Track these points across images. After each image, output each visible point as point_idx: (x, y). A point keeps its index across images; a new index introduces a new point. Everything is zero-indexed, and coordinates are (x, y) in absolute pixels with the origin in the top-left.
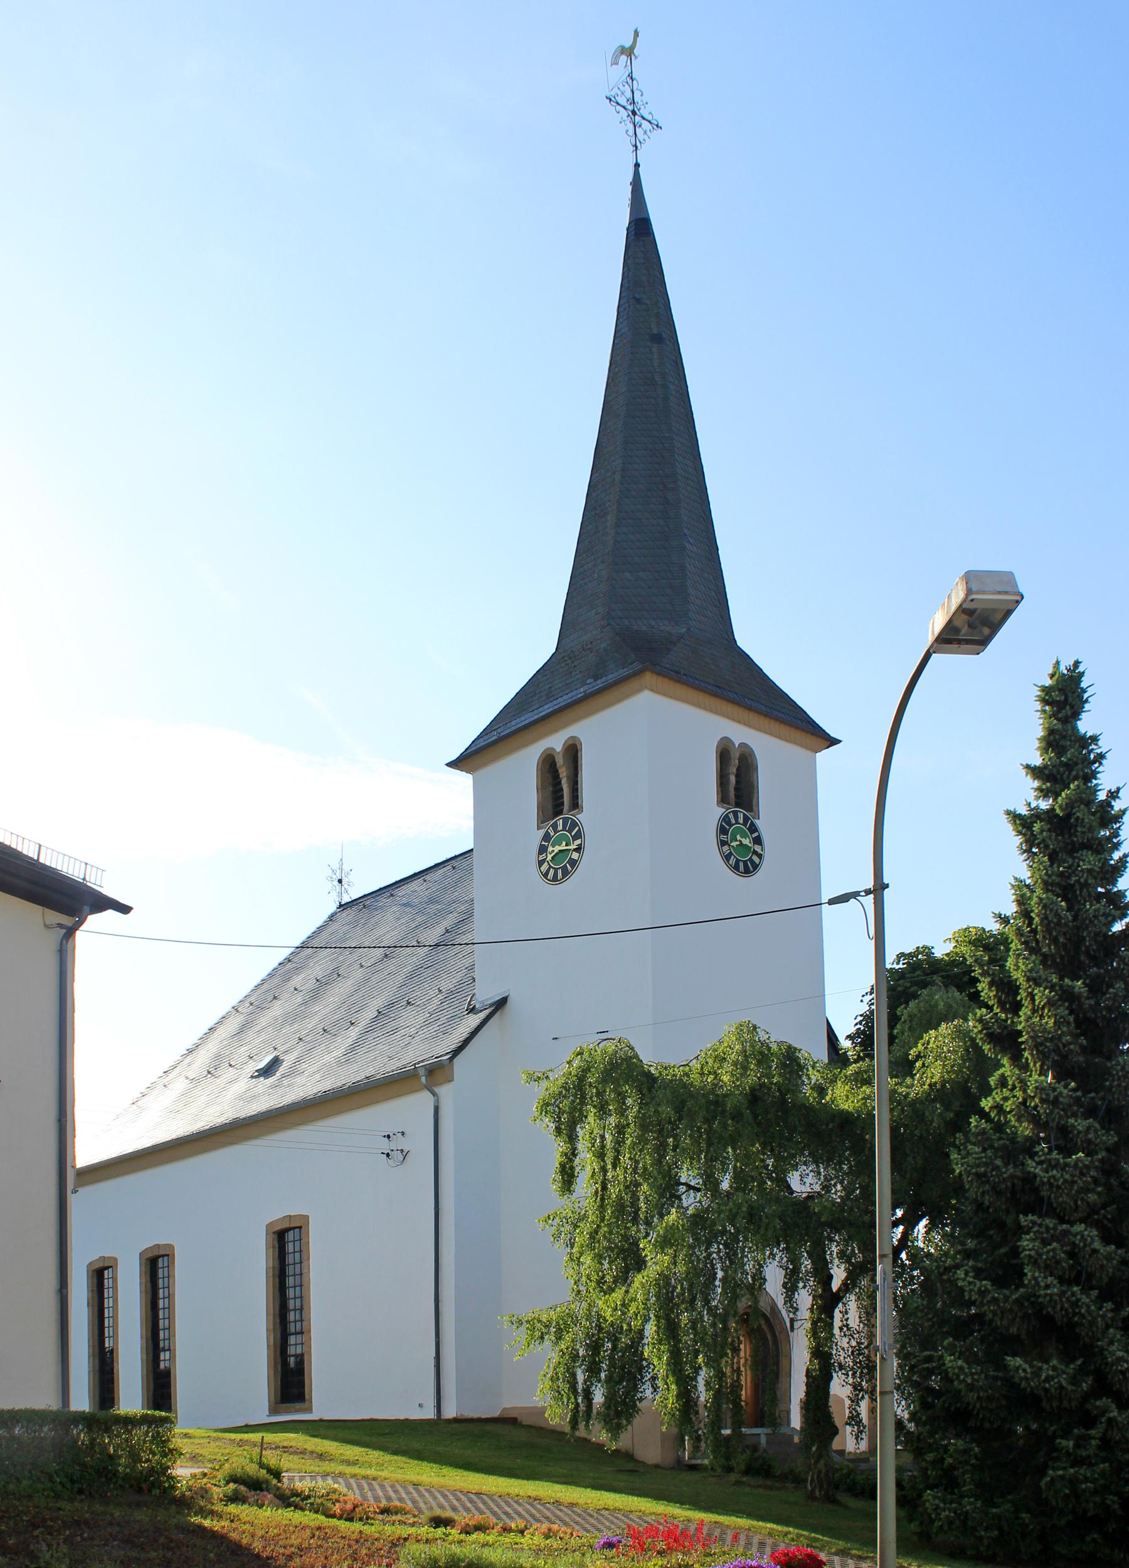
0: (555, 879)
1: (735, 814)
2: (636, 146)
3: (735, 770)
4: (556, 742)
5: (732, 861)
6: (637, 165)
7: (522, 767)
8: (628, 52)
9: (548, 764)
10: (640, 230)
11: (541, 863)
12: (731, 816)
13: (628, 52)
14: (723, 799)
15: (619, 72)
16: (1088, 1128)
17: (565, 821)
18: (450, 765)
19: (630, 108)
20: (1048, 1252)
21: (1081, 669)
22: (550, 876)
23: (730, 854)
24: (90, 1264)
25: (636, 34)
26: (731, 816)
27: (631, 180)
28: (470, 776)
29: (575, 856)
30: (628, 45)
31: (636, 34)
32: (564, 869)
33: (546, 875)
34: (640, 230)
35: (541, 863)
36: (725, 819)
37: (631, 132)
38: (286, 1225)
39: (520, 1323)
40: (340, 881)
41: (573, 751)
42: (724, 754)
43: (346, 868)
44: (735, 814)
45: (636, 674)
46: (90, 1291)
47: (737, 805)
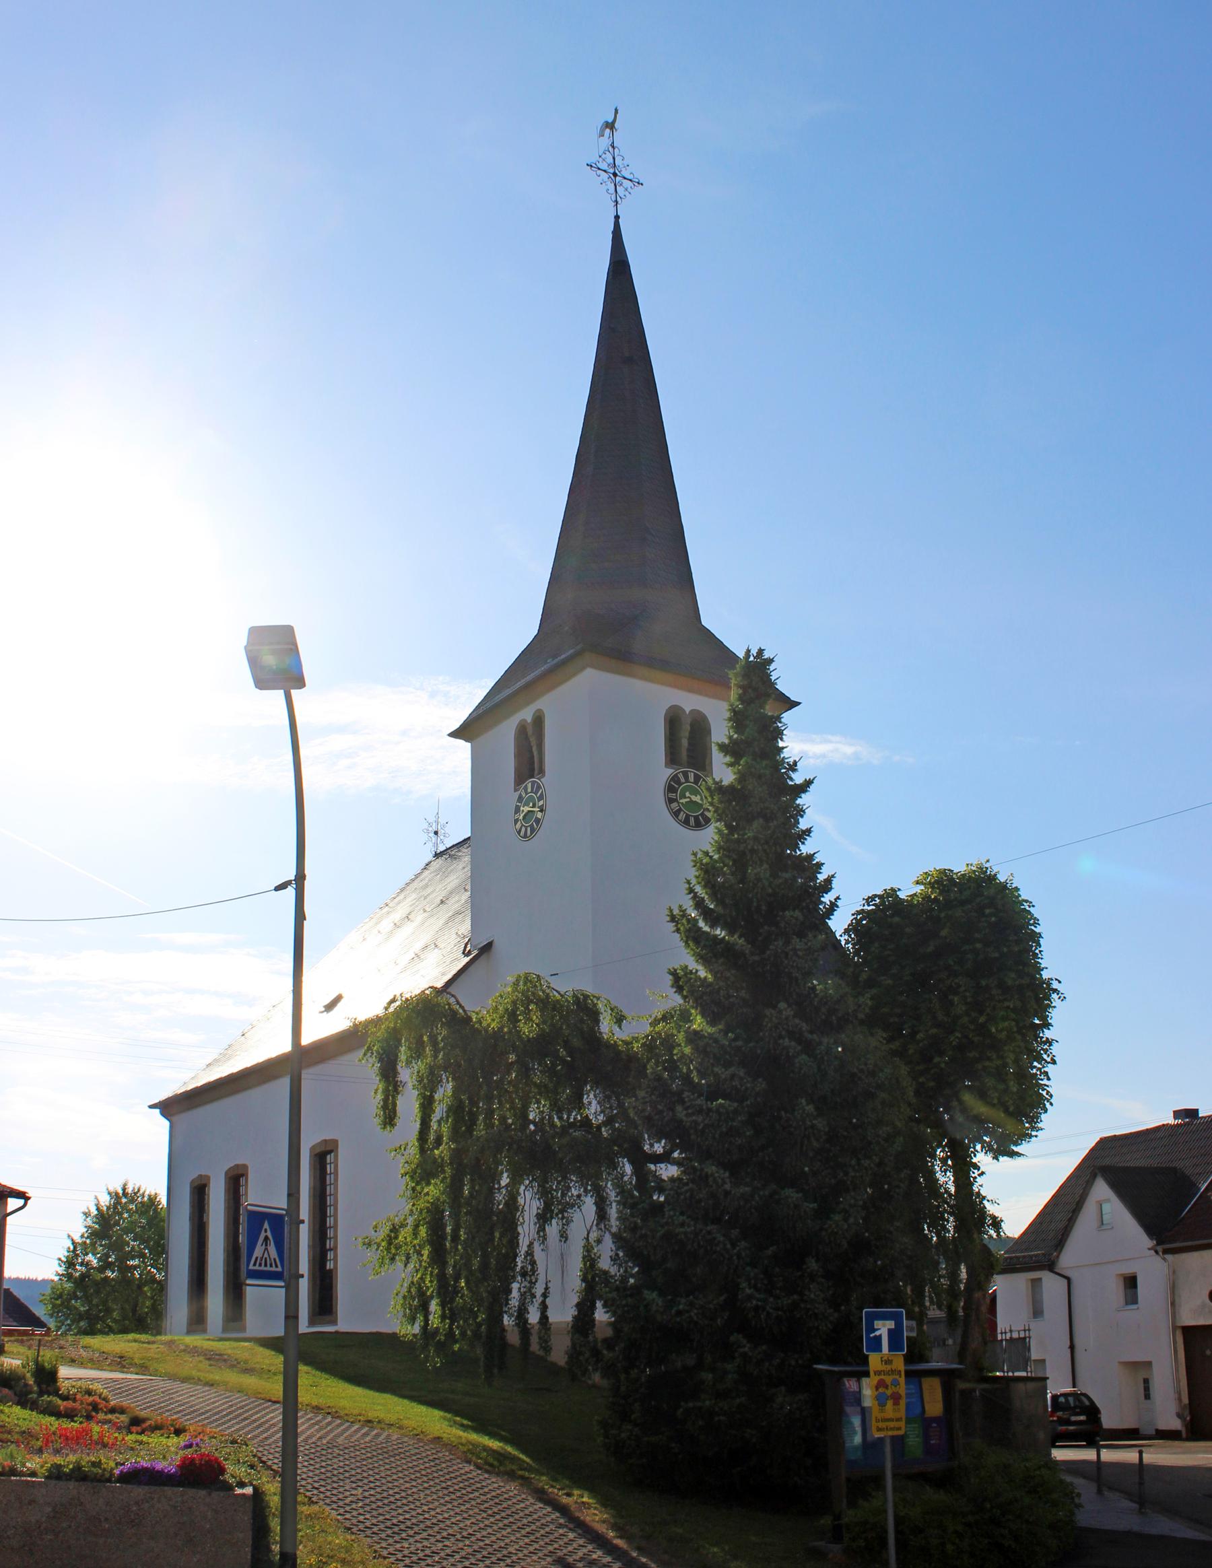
0: (525, 836)
1: (685, 774)
2: (616, 202)
3: (687, 734)
4: (527, 714)
5: (682, 816)
6: (617, 217)
7: (505, 734)
8: (611, 126)
9: (522, 730)
10: (619, 269)
11: (516, 821)
12: (680, 776)
13: (611, 126)
14: (672, 758)
15: (605, 142)
16: (733, 1076)
17: (533, 783)
18: (455, 734)
19: (612, 171)
20: (687, 1191)
21: (766, 655)
22: (522, 833)
23: (680, 810)
24: (192, 1182)
25: (616, 111)
26: (680, 776)
27: (612, 229)
28: (469, 745)
29: (539, 815)
30: (610, 120)
31: (616, 111)
32: (532, 826)
33: (519, 832)
34: (619, 269)
35: (516, 821)
36: (675, 778)
37: (612, 190)
38: (323, 1149)
39: (369, 1244)
40: (436, 833)
41: (539, 720)
42: (673, 720)
43: (442, 821)
44: (685, 774)
45: (578, 654)
46: (192, 1206)
47: (690, 765)
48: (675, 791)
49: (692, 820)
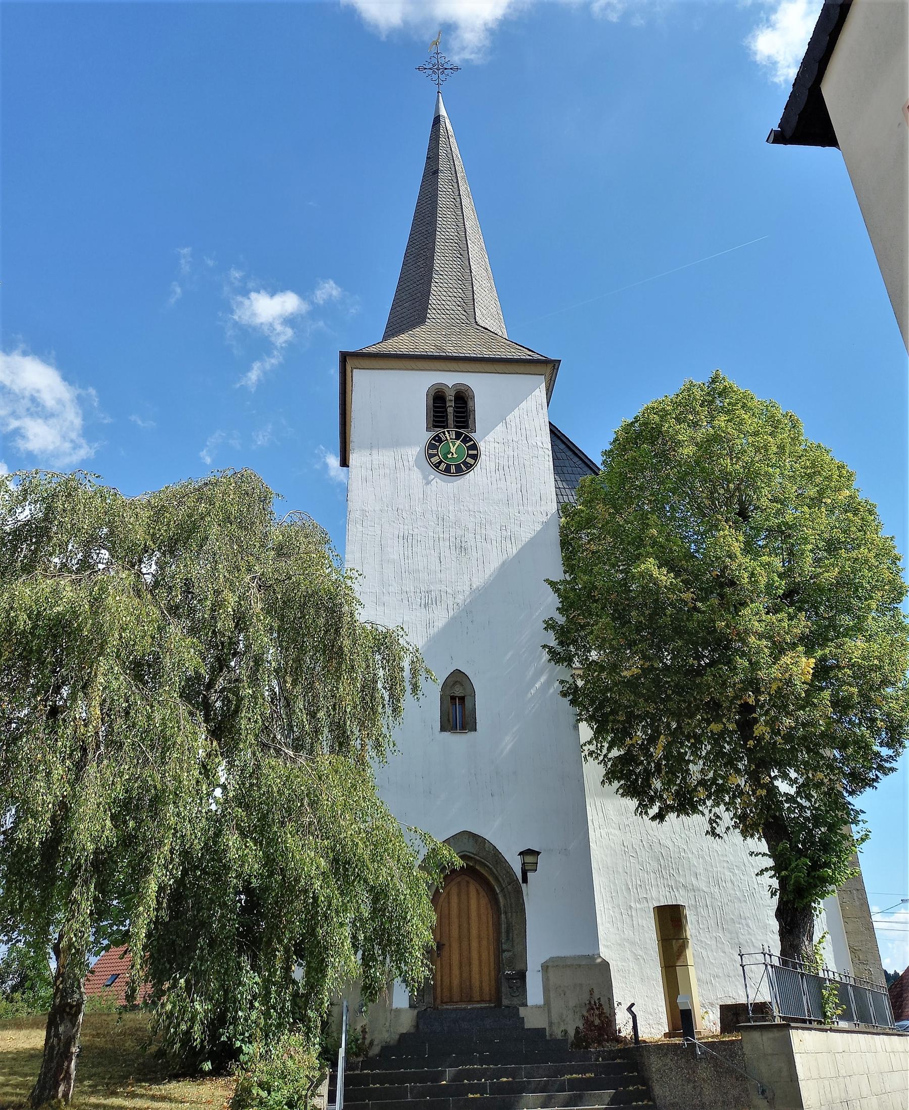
48: (436, 448)
49: (453, 469)
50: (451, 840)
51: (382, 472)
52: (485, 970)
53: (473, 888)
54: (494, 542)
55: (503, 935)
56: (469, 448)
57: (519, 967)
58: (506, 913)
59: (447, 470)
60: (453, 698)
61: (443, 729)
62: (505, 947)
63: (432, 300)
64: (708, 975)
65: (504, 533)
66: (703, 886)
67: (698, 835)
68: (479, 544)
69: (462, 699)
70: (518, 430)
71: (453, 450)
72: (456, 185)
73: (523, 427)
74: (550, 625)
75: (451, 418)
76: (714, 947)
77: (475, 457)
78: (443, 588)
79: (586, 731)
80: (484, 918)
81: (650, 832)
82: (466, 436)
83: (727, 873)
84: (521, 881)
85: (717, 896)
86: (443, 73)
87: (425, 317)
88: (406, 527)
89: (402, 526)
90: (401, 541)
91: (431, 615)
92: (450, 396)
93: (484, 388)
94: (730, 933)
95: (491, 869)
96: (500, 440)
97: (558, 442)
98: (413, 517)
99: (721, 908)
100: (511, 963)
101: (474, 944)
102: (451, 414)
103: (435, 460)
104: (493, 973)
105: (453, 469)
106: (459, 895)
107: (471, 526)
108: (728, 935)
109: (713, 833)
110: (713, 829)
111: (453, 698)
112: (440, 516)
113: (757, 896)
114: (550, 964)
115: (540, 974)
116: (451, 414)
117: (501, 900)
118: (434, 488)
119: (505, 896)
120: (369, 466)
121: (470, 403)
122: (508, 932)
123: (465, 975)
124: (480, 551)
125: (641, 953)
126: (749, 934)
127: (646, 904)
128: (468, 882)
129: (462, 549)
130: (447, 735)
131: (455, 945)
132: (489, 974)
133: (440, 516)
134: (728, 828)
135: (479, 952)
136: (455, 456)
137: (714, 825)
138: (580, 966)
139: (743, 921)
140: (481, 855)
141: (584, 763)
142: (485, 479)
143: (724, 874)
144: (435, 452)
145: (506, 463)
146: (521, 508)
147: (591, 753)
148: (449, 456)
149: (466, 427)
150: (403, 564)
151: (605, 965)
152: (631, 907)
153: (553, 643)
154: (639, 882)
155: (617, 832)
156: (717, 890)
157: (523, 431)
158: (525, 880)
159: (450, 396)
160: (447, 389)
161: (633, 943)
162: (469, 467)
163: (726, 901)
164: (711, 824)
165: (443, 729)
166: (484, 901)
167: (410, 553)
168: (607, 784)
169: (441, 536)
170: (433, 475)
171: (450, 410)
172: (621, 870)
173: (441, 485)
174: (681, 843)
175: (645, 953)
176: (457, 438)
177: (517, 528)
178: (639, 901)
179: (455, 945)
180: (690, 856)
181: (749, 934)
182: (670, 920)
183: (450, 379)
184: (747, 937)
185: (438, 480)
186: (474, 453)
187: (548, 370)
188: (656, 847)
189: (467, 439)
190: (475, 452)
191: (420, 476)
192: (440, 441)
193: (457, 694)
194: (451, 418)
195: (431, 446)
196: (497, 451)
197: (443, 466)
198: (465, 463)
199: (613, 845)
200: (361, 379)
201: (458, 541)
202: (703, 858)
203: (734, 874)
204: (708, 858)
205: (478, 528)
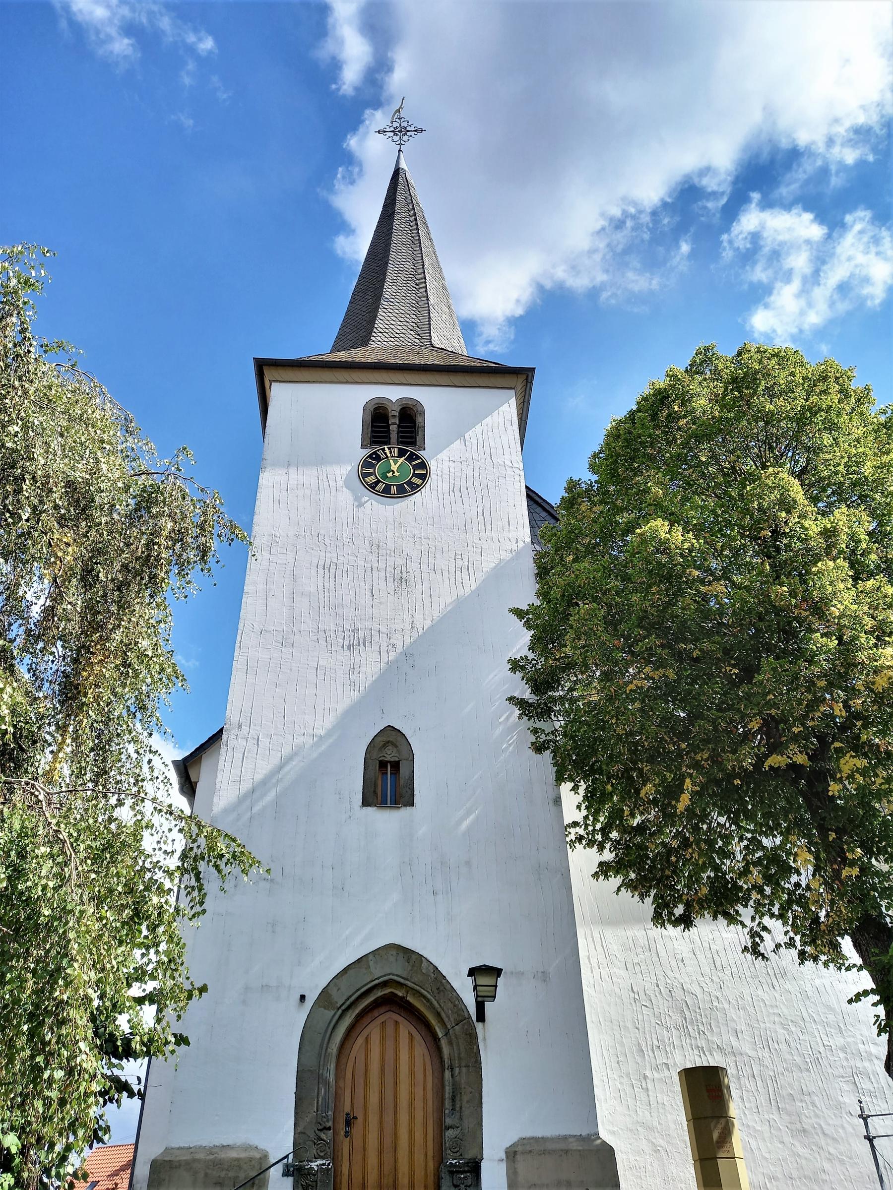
48: (374, 466)
49: (394, 489)
50: (371, 957)
51: (300, 493)
52: (419, 1157)
53: (406, 1029)
54: (446, 574)
55: (448, 1104)
56: (415, 467)
57: (470, 1154)
58: (452, 1069)
59: (386, 491)
60: (383, 765)
61: (366, 803)
62: (448, 1121)
63: (378, 324)
64: (761, 1177)
65: (459, 562)
66: (747, 1049)
67: (737, 979)
68: (425, 576)
69: (396, 766)
70: (480, 447)
71: (394, 467)
72: (414, 226)
73: (486, 444)
74: (516, 665)
75: (394, 436)
76: (767, 1135)
77: (423, 477)
78: (375, 626)
79: (572, 802)
80: (419, 1076)
81: (669, 973)
82: (412, 454)
83: (781, 1031)
84: (474, 1018)
85: (767, 1062)
86: (404, 135)
87: (369, 339)
88: (328, 555)
89: (323, 554)
90: (321, 571)
91: (357, 658)
92: (394, 411)
93: (436, 403)
94: (789, 1114)
95: (428, 1000)
96: (457, 458)
97: (539, 510)
98: (339, 543)
99: (774, 1079)
100: (458, 1146)
101: (404, 1117)
102: (394, 432)
103: (371, 479)
104: (431, 1165)
105: (394, 489)
106: (383, 1038)
107: (415, 554)
108: (784, 1116)
109: (755, 950)
110: (755, 945)
111: (383, 765)
112: (376, 542)
113: (824, 1062)
114: (519, 1149)
115: (503, 1166)
116: (394, 432)
117: (446, 1050)
118: (368, 511)
119: (450, 1043)
120: (284, 486)
121: (419, 419)
122: (453, 1099)
123: (387, 1169)
124: (426, 584)
125: (662, 1142)
126: (817, 1116)
127: (667, 1073)
128: (396, 1022)
129: (402, 580)
130: (371, 812)
131: (373, 1120)
132: (426, 1166)
133: (376, 542)
134: (778, 946)
135: (411, 1132)
136: (396, 474)
137: (757, 939)
138: (567, 1152)
139: (807, 1098)
140: (416, 980)
141: (569, 851)
142: (435, 502)
143: (776, 1032)
144: (371, 470)
145: (463, 484)
146: (483, 534)
147: (580, 839)
148: (390, 475)
149: (414, 443)
150: (321, 596)
151: (607, 1154)
152: (645, 1077)
153: (527, 694)
154: (655, 1042)
155: (623, 973)
156: (767, 1055)
157: (487, 449)
158: (481, 1016)
159: (394, 411)
160: (390, 404)
161: (651, 1129)
162: (415, 488)
163: (780, 1069)
164: (752, 937)
165: (366, 803)
166: (421, 1048)
167: (332, 584)
168: (602, 878)
169: (375, 565)
170: (368, 497)
171: (394, 428)
172: (630, 1025)
173: (378, 509)
174: (711, 988)
175: (668, 1142)
176: (400, 456)
177: (478, 557)
178: (657, 1068)
179: (373, 1120)
180: (726, 1006)
181: (817, 1116)
182: (705, 1091)
183: (394, 393)
184: (814, 1120)
185: (373, 502)
186: (422, 472)
187: (519, 382)
188: (678, 993)
189: (412, 457)
190: (424, 471)
191: (350, 497)
192: (378, 459)
193: (388, 758)
194: (394, 436)
195: (366, 464)
196: (452, 470)
197: (381, 487)
198: (409, 483)
199: (617, 990)
200: (279, 393)
201: (397, 571)
202: (744, 1009)
203: (790, 1032)
204: (751, 1010)
205: (424, 557)
